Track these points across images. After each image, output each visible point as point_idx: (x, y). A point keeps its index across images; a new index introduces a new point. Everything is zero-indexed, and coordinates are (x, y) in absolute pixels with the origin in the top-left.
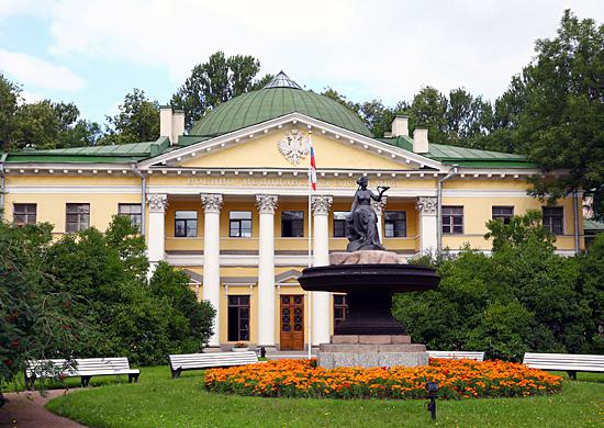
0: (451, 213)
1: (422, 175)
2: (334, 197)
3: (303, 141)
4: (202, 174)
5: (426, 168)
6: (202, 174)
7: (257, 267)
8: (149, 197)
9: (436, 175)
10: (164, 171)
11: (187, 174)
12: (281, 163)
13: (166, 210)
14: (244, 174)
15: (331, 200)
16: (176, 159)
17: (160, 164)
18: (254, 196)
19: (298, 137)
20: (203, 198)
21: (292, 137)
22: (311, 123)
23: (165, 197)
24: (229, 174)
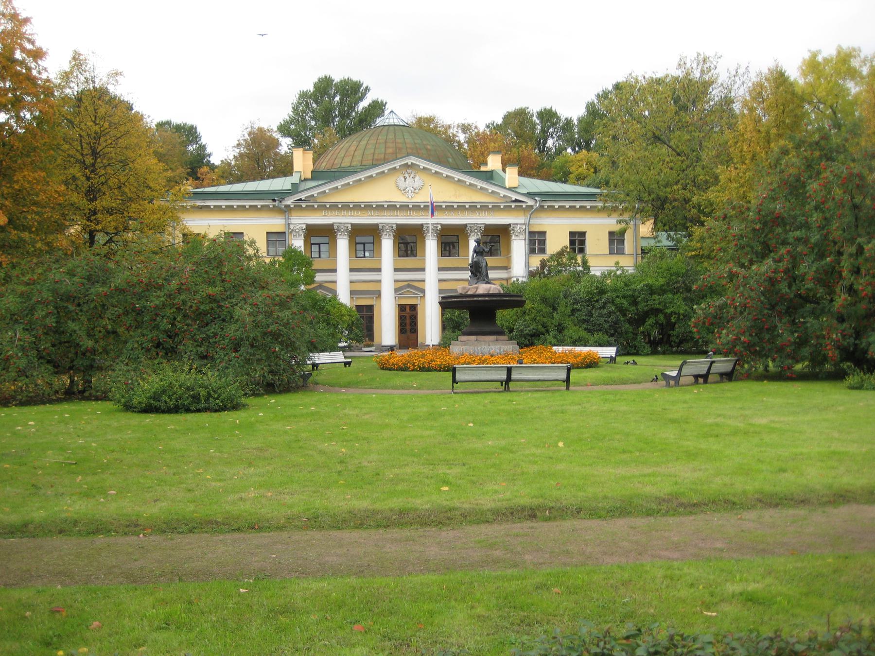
1: (513, 207)
2: (442, 225)
3: (417, 179)
4: (334, 207)
5: (516, 201)
6: (334, 207)
8: (292, 227)
9: (524, 206)
10: (304, 205)
11: (322, 208)
12: (399, 198)
13: (305, 237)
14: (369, 207)
15: (439, 227)
16: (313, 196)
17: (300, 200)
18: (377, 225)
19: (412, 176)
20: (336, 227)
21: (407, 175)
22: (423, 164)
23: (304, 227)
24: (357, 207)
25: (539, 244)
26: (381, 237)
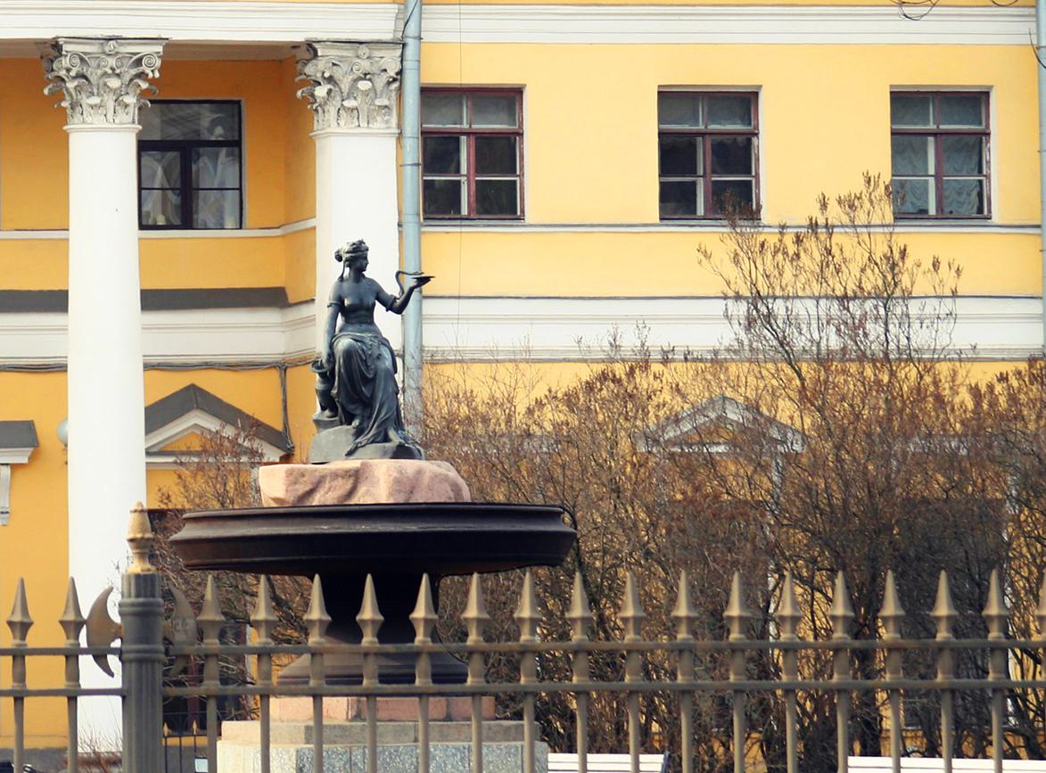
0: (466, 121)
7: (61, 368)
25: (482, 165)
26: (63, 117)
